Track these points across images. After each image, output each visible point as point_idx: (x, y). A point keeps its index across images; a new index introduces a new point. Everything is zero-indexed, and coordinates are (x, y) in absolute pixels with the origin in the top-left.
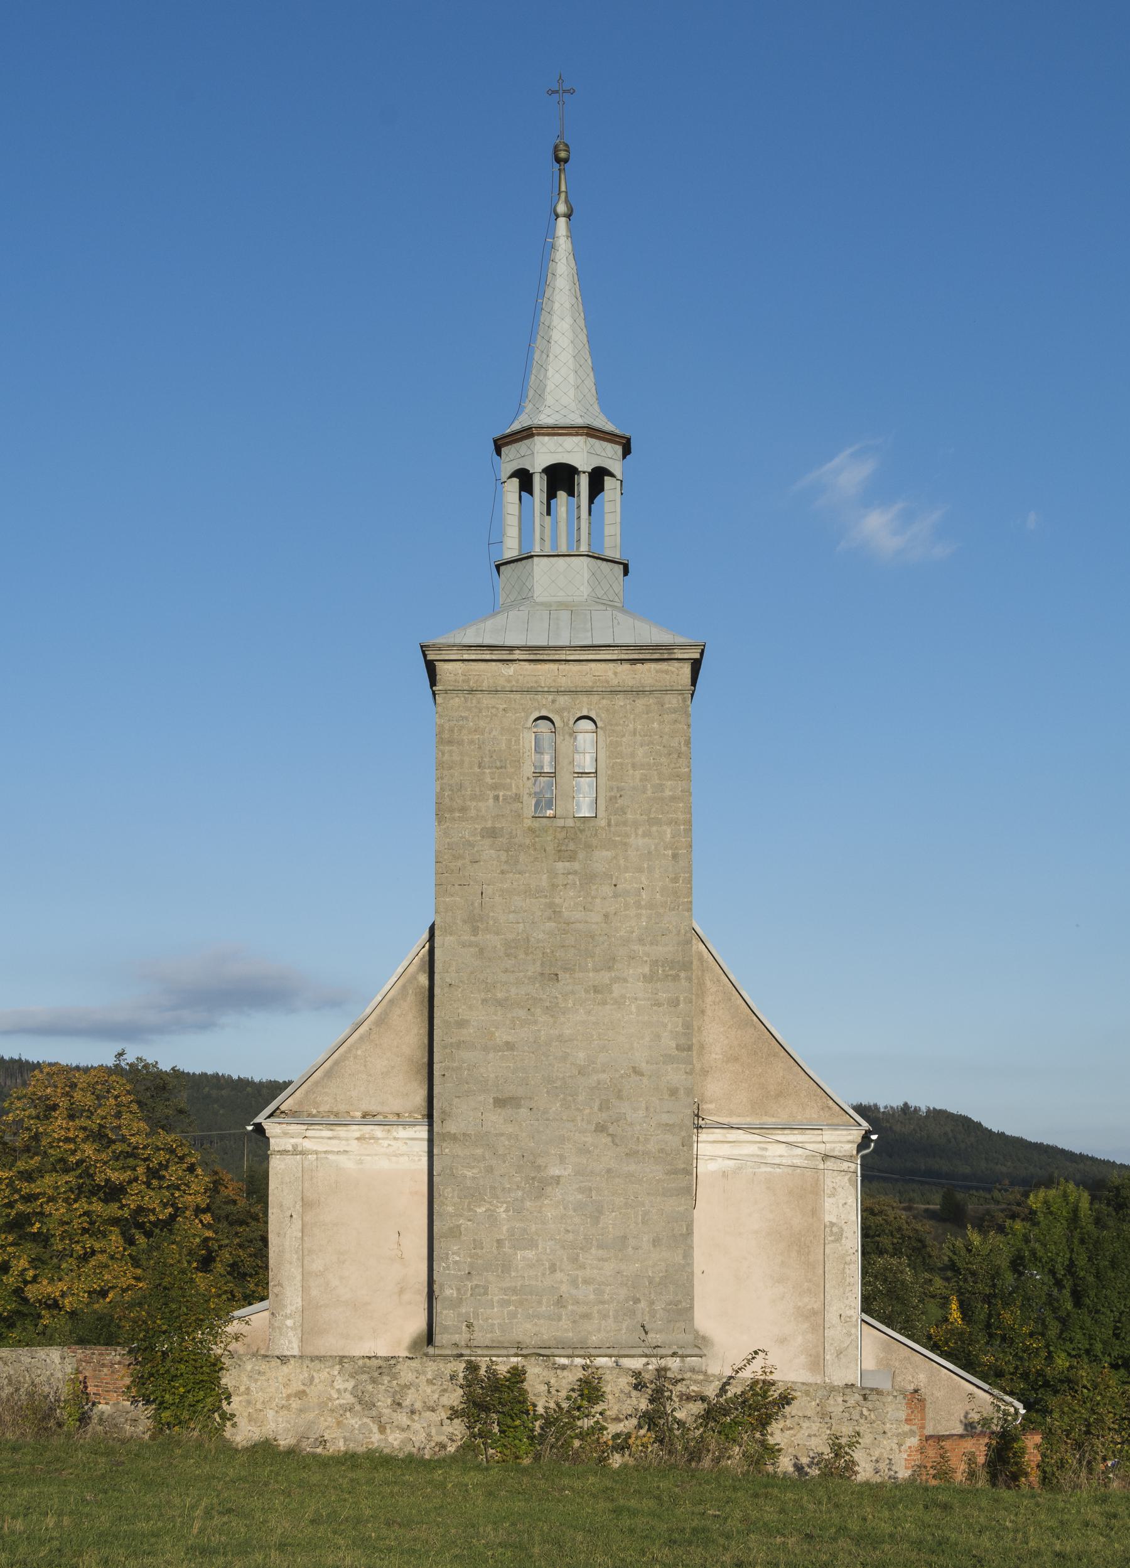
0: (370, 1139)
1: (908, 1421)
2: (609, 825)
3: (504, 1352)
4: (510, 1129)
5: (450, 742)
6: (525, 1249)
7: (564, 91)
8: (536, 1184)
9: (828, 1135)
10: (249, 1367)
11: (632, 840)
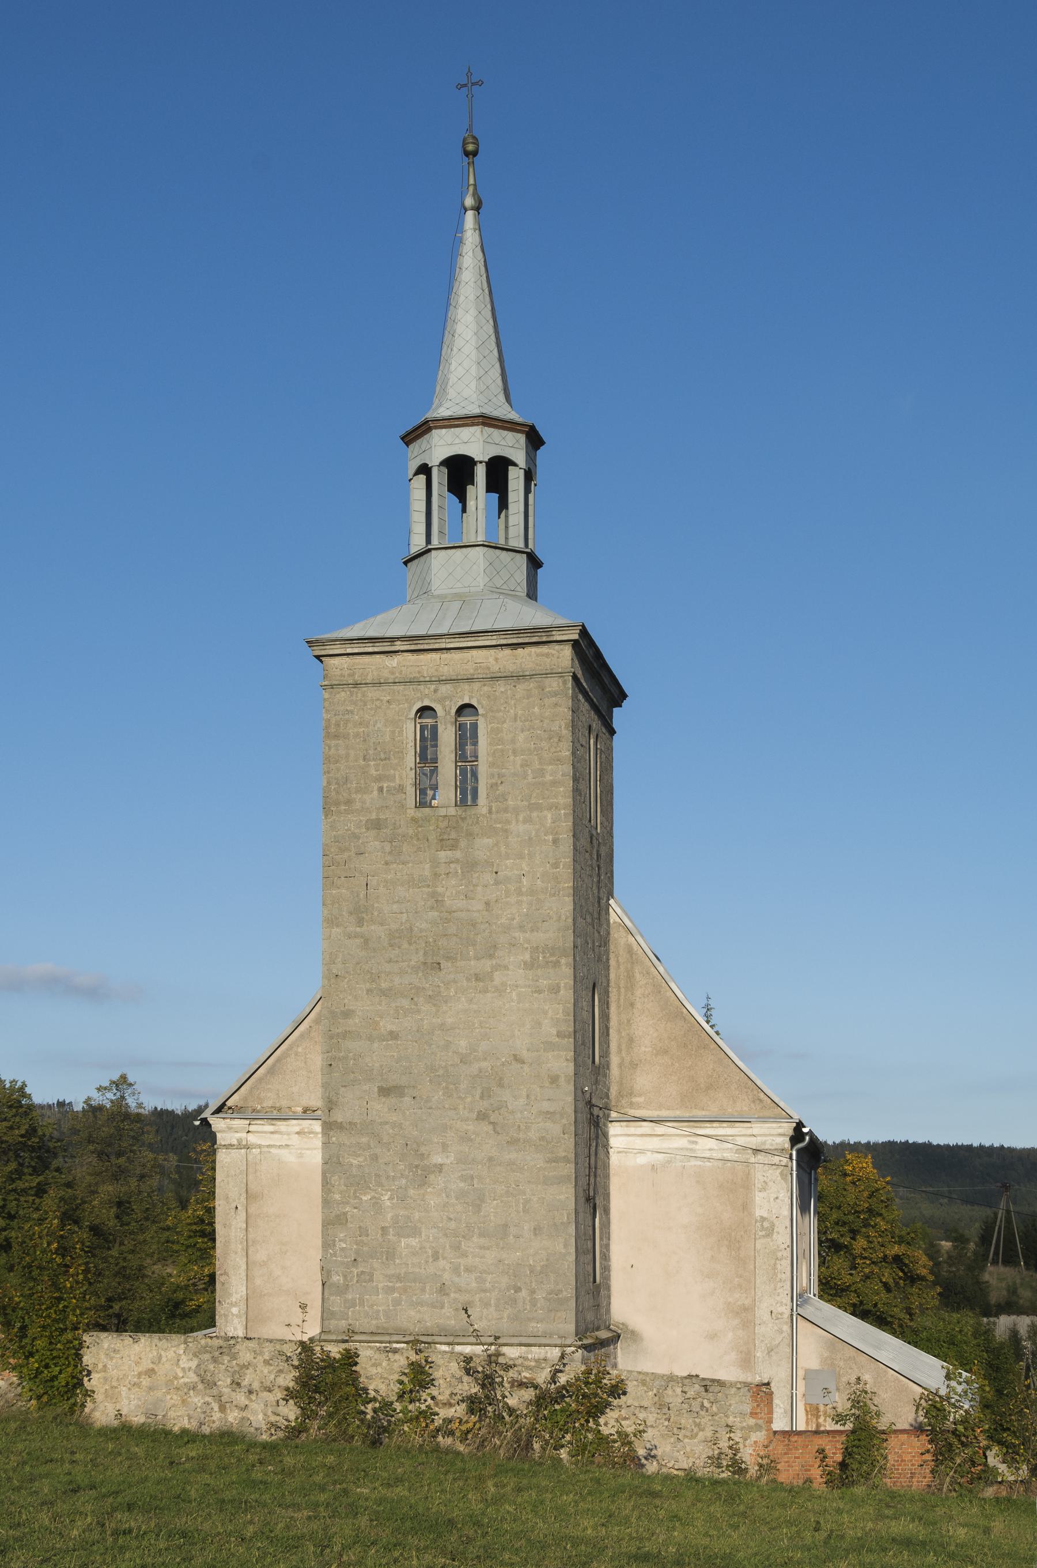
0: (310, 1133)
1: (753, 1414)
2: (490, 812)
3: (387, 1338)
4: (394, 1118)
5: (336, 736)
6: (408, 1236)
7: (473, 84)
8: (420, 1172)
9: (757, 1128)
10: (106, 1345)
11: (513, 827)
